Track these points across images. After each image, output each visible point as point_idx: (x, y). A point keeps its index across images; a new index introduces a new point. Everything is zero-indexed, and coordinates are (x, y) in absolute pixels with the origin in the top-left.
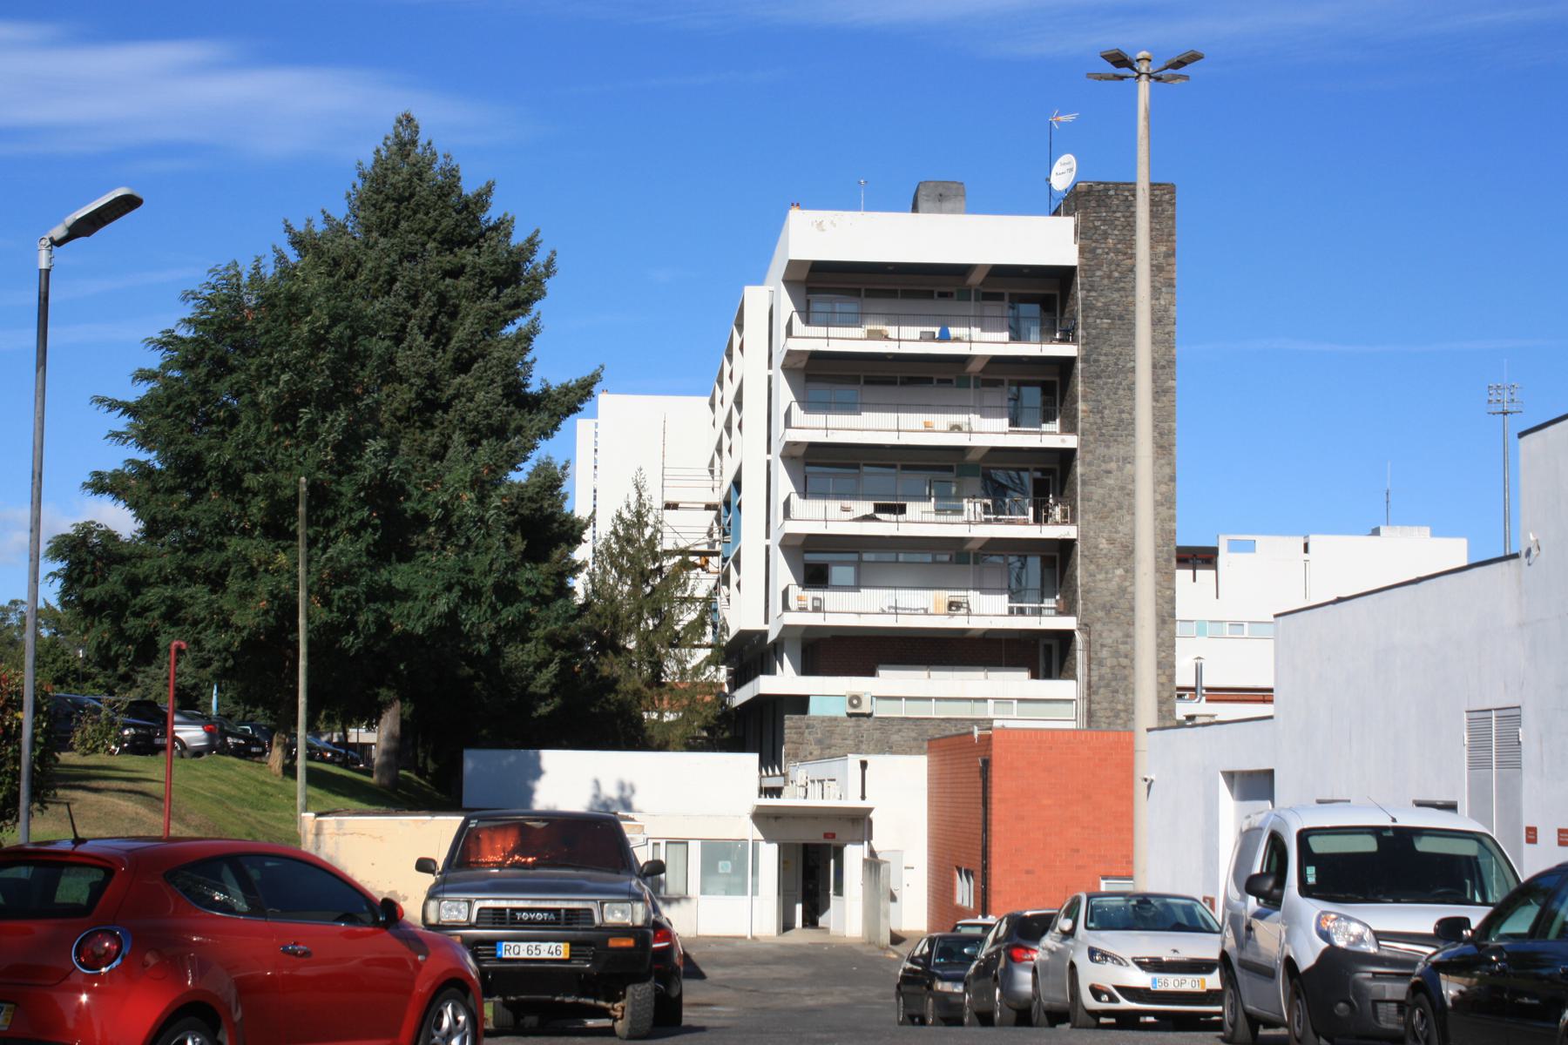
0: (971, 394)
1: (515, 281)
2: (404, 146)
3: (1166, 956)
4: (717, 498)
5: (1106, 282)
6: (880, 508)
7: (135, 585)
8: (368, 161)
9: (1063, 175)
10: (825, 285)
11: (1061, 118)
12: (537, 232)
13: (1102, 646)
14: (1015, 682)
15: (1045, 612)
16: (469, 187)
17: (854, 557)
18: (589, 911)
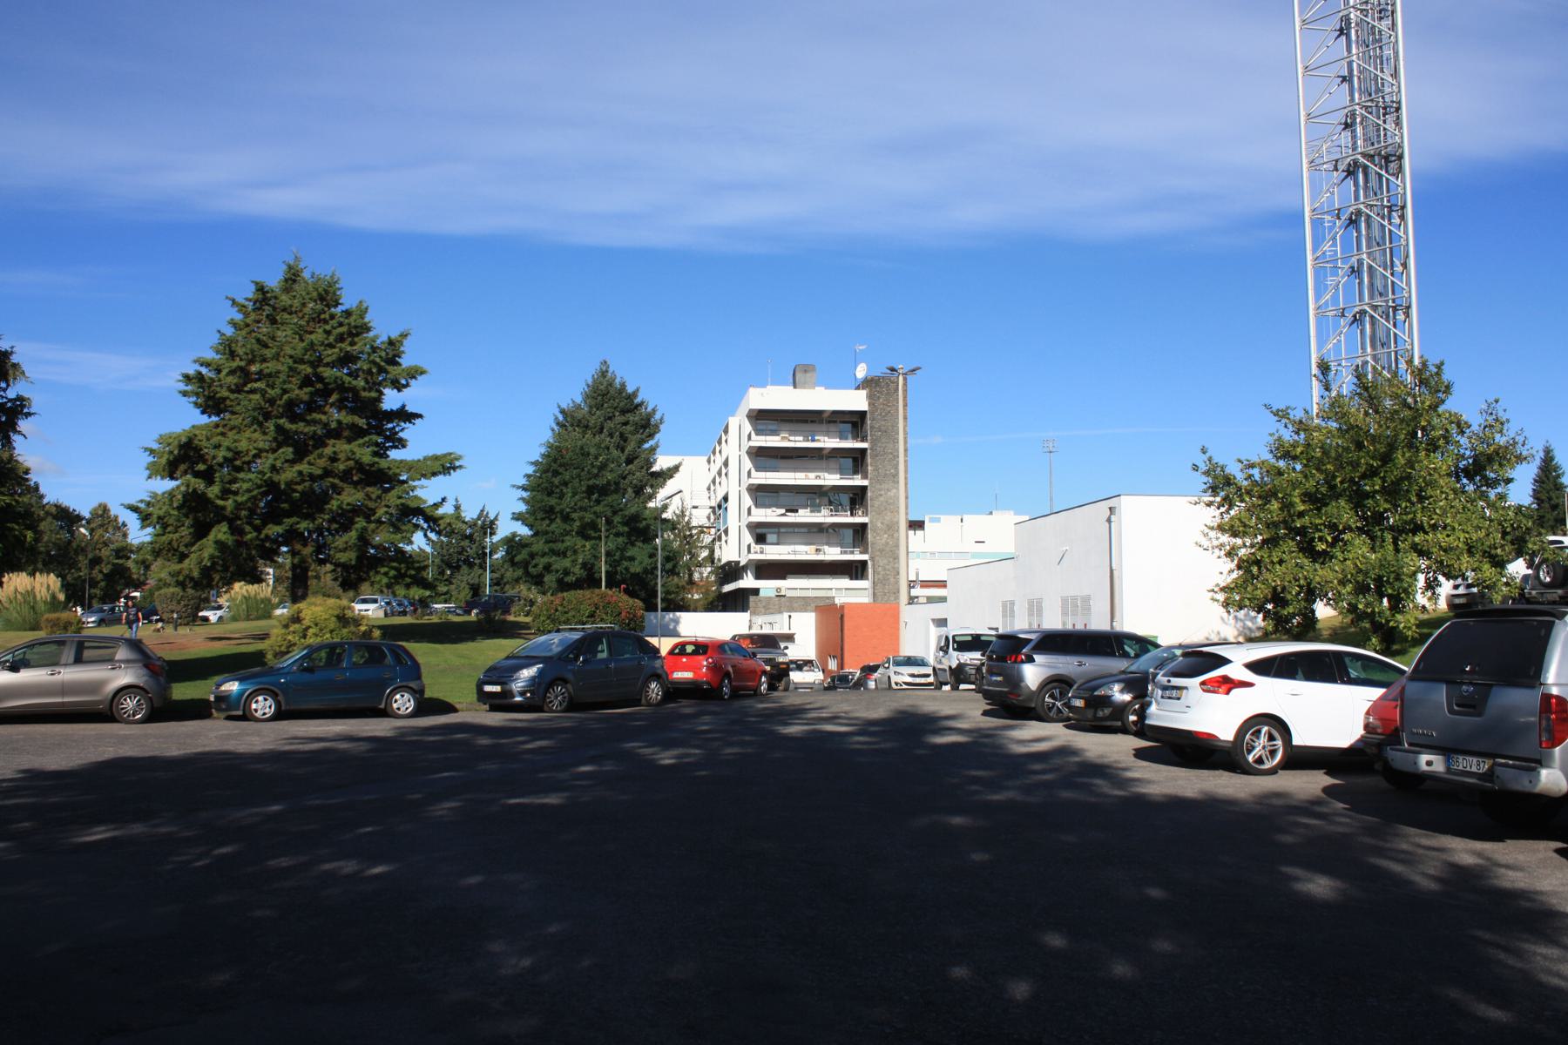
1: (648, 427)
2: (604, 374)
4: (714, 504)
8: (590, 381)
9: (861, 372)
10: (764, 419)
14: (845, 582)
16: (630, 389)
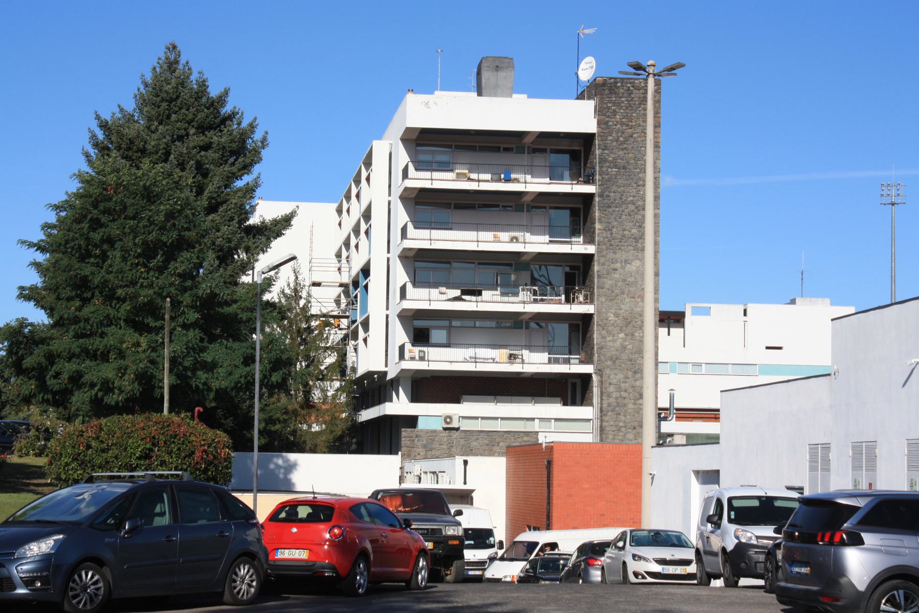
0: (524, 217)
1: (242, 152)
2: (172, 65)
3: (668, 557)
5: (614, 144)
6: (464, 292)
7: (51, 358)
9: (587, 71)
11: (586, 31)
12: (255, 118)
13: (610, 384)
14: (554, 409)
15: (572, 361)
16: (214, 91)
17: (446, 323)
18: (440, 530)
